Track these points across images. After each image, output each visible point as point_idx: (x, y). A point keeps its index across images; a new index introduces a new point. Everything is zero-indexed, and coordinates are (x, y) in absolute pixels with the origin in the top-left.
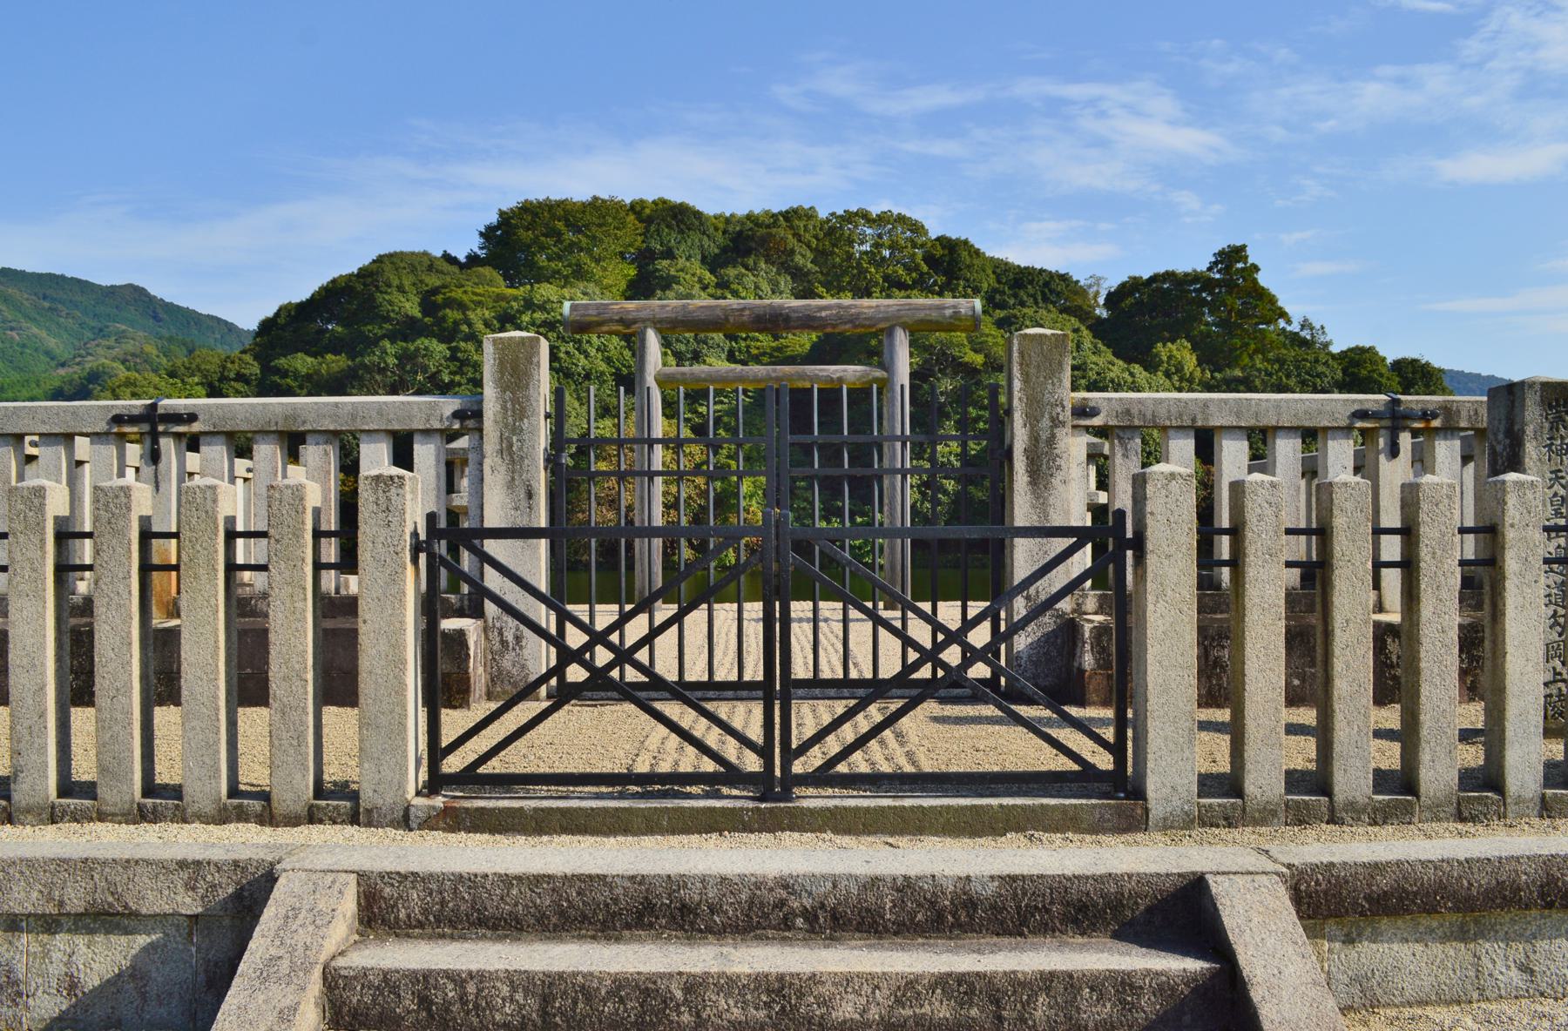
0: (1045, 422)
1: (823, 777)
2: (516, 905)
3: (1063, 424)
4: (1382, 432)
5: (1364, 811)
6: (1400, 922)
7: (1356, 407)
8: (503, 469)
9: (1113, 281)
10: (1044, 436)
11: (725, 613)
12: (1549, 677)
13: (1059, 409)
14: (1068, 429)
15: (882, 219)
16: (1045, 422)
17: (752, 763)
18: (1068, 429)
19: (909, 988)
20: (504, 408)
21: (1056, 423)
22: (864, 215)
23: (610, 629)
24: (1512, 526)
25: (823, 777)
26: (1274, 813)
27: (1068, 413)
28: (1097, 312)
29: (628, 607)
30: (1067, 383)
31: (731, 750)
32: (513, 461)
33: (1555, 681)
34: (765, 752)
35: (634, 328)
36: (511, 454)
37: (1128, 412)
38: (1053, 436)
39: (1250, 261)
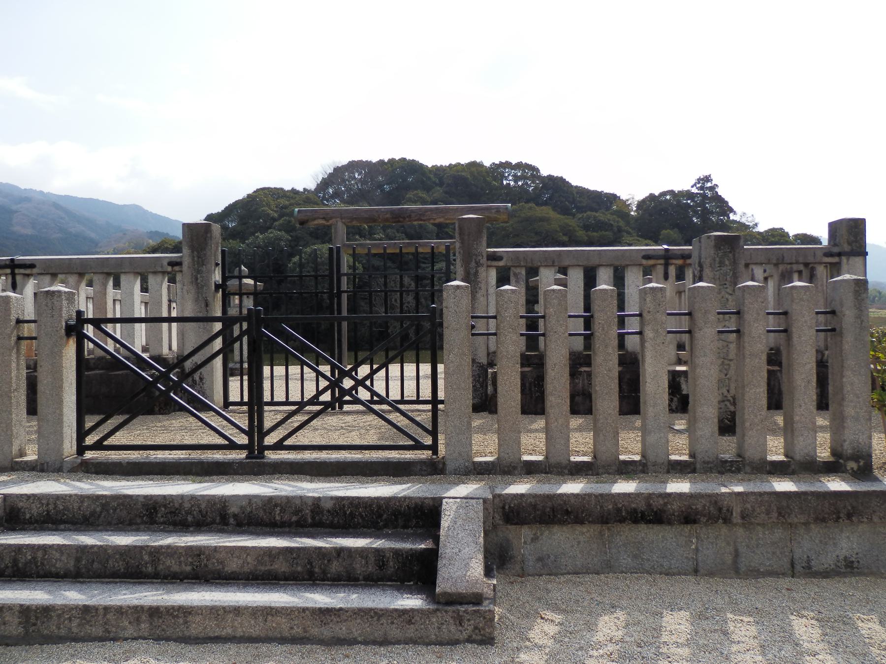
0: (473, 264)
1: (279, 446)
2: (48, 504)
3: (482, 265)
4: (659, 267)
5: (565, 467)
6: (564, 528)
7: (644, 253)
8: (193, 291)
9: (641, 195)
10: (472, 271)
11: (410, 369)
12: (720, 398)
13: (480, 258)
14: (484, 268)
15: (519, 166)
16: (473, 264)
17: (243, 440)
18: (484, 268)
19: (269, 552)
20: (193, 259)
21: (478, 264)
22: (507, 165)
23: (366, 378)
24: (649, 312)
25: (279, 446)
26: (515, 468)
27: (485, 259)
28: (632, 213)
29: (375, 367)
30: (484, 243)
31: (230, 432)
32: (198, 288)
33: (723, 401)
34: (249, 433)
35: (331, 222)
36: (197, 284)
37: (518, 258)
38: (477, 272)
39: (714, 183)
